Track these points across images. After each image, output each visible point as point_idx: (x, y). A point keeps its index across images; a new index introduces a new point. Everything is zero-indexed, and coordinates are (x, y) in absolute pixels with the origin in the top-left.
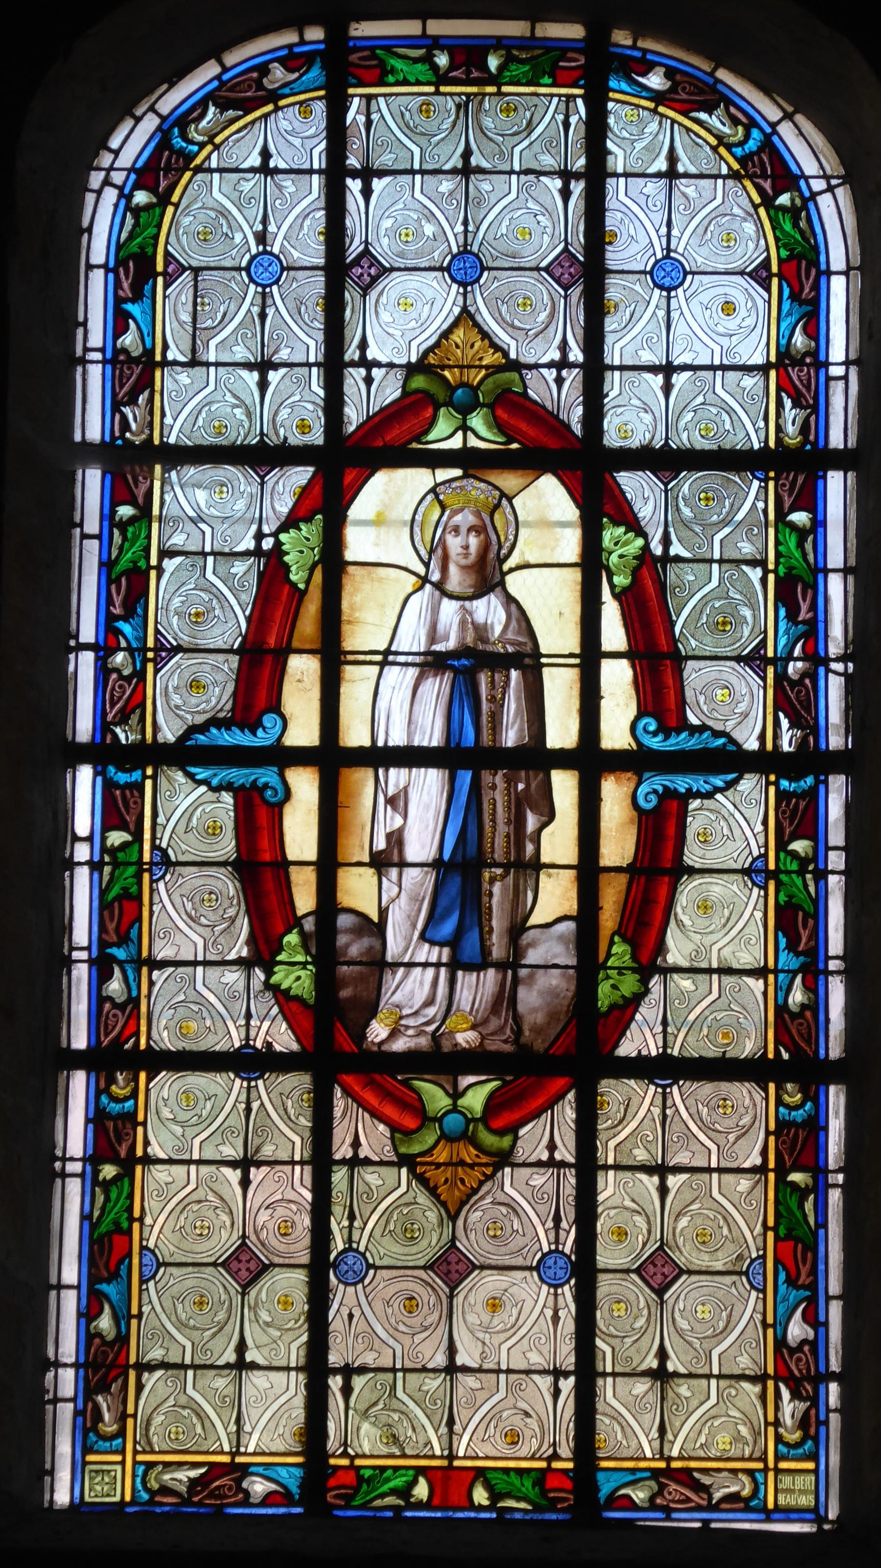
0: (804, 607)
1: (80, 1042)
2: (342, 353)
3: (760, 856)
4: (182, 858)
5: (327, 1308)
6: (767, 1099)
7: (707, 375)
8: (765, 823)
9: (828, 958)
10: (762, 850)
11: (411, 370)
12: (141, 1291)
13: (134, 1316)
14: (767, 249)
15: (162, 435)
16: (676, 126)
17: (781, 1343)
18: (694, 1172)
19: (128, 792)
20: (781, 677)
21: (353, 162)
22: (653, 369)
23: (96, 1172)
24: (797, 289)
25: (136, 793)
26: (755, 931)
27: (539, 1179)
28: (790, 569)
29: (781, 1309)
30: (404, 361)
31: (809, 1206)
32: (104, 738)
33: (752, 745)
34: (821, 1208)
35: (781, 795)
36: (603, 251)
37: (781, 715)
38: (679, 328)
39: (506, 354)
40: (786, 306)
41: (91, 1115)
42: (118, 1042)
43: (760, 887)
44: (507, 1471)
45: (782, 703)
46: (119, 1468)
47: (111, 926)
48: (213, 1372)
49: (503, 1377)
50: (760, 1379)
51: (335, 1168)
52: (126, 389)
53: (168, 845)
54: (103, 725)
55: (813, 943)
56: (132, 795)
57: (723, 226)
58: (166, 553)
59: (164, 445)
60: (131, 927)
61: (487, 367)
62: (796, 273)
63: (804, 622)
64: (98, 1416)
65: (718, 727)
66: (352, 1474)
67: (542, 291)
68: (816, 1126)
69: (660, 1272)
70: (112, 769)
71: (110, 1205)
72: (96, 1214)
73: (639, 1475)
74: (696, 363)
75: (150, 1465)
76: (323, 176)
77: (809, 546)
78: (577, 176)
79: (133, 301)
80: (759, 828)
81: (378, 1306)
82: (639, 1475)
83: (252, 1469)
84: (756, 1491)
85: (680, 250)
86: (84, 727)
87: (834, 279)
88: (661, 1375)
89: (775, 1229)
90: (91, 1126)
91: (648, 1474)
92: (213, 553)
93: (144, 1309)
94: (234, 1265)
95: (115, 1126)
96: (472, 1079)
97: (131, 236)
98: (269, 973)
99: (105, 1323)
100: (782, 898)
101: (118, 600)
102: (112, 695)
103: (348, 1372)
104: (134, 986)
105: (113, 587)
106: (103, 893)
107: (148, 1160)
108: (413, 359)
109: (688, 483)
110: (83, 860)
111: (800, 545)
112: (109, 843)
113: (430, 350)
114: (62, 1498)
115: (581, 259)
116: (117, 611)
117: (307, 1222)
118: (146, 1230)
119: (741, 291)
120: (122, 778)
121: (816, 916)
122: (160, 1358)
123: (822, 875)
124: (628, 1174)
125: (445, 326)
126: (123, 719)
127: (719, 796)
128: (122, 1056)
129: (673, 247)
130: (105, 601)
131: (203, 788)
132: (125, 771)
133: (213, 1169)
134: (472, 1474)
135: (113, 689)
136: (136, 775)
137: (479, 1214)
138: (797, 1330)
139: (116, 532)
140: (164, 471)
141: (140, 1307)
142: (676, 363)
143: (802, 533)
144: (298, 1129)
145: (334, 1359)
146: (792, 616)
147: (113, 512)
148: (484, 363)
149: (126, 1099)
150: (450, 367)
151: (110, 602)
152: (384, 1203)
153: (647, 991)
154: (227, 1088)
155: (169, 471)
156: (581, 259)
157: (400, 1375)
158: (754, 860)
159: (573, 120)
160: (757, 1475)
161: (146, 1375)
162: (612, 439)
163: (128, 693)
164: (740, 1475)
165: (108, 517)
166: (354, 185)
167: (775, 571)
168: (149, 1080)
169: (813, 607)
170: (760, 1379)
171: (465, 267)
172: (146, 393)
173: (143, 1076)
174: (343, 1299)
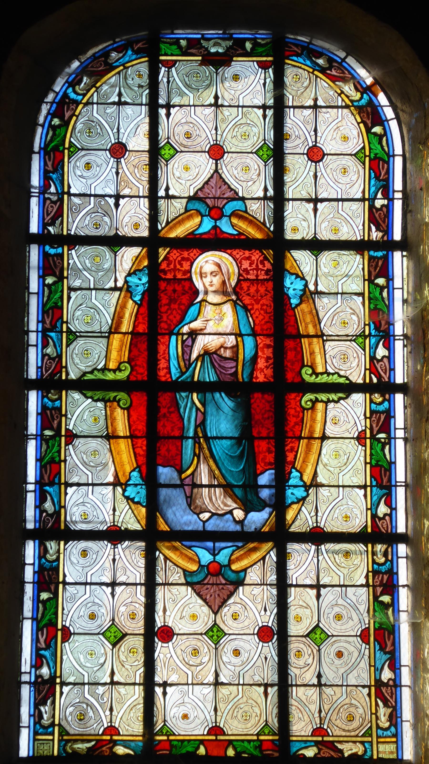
0: (389, 644)
1: (32, 374)
2: (157, 193)
3: (362, 431)
4: (76, 631)
5: (154, 651)
6: (364, 168)
7: (335, 204)
8: (364, 225)
9: (394, 191)
10: (364, 428)
11: (190, 199)
12: (65, 450)
13: (63, 461)
14: (364, 142)
15: (68, 230)
16: (319, 79)
17: (374, 516)
18: (332, 589)
19: (53, 412)
20: (372, 207)
21: (161, 101)
22: (311, 586)
23: (44, 280)
24: (378, 174)
25: (57, 412)
26: (360, 465)
27: (257, 590)
28: (376, 154)
29: (375, 498)
30: (186, 195)
31: (385, 294)
32: (43, 231)
33: (360, 381)
34: (391, 296)
35: (371, 258)
36: (283, 177)
37: (372, 225)
38: (321, 181)
39: (237, 194)
40: (373, 182)
41: (39, 411)
42: (53, 374)
43: (362, 446)
44: (243, 741)
45: (372, 219)
46: (51, 743)
47: (42, 640)
48: (104, 292)
49: (240, 109)
50: (364, 487)
51: (159, 200)
52: (49, 217)
53: (70, 625)
54: (44, 225)
55: (386, 176)
56: (58, 259)
57: (341, 132)
58: (71, 289)
59: (69, 235)
60: (51, 641)
61: (227, 198)
62: (378, 166)
63: (383, 180)
64: (41, 716)
65: (342, 373)
66: (168, 742)
67: (255, 163)
68: (389, 415)
69: (317, 634)
70: (47, 248)
71: (46, 612)
72: (40, 616)
73: (308, 744)
74: (329, 197)
75: (68, 741)
76: (147, 107)
77: (384, 143)
78: (270, 107)
79: (45, 649)
80: (361, 227)
81: (179, 652)
82: (308, 744)
83: (118, 742)
84: (366, 751)
85: (322, 142)
86: (34, 227)
87: (396, 158)
88: (318, 587)
89: (370, 463)
90: (39, 417)
91: (313, 744)
92: (89, 684)
93: (67, 458)
94: (108, 634)
95: (48, 574)
96: (223, 544)
97: (51, 141)
98: (124, 491)
99: (48, 505)
100: (372, 306)
101: (42, 640)
102: (46, 367)
103: (165, 685)
104: (59, 349)
105: (40, 633)
106: (44, 305)
107: (68, 485)
108: (192, 194)
109: (327, 257)
110: (29, 581)
111: (380, 143)
112: (47, 282)
113: (201, 189)
114: (23, 752)
115: (272, 147)
116: (50, 168)
117: (147, 224)
118: (68, 421)
119: (352, 164)
120: (52, 251)
121: (390, 470)
122: (79, 284)
123: (397, 612)
124: (302, 589)
125: (206, 179)
126: (53, 224)
127: (342, 401)
128: (53, 382)
129: (318, 141)
130: (36, 640)
131: (90, 400)
132: (54, 248)
133: (97, 585)
134: (226, 744)
135: (46, 363)
136: (60, 250)
137: (227, 608)
138: (383, 509)
139: (40, 605)
140: (69, 250)
141: (65, 457)
142: (319, 197)
143: (380, 137)
144: (138, 569)
145: (158, 679)
146: (377, 177)
147: (39, 596)
148: (225, 196)
149: (56, 400)
150: (210, 198)
151: (38, 640)
152: (181, 607)
153: (308, 495)
154: (104, 548)
155: (71, 250)
156: (272, 147)
157: (190, 682)
158: (359, 433)
159: (268, 80)
160: (366, 745)
161: (69, 488)
162: (289, 235)
163: (53, 366)
164: (357, 744)
165: (43, 285)
166: (162, 112)
167: (370, 463)
168: (65, 545)
169: (393, 644)
170: (364, 487)
171: (217, 152)
172: (51, 699)
173: (62, 543)
174: (161, 650)
